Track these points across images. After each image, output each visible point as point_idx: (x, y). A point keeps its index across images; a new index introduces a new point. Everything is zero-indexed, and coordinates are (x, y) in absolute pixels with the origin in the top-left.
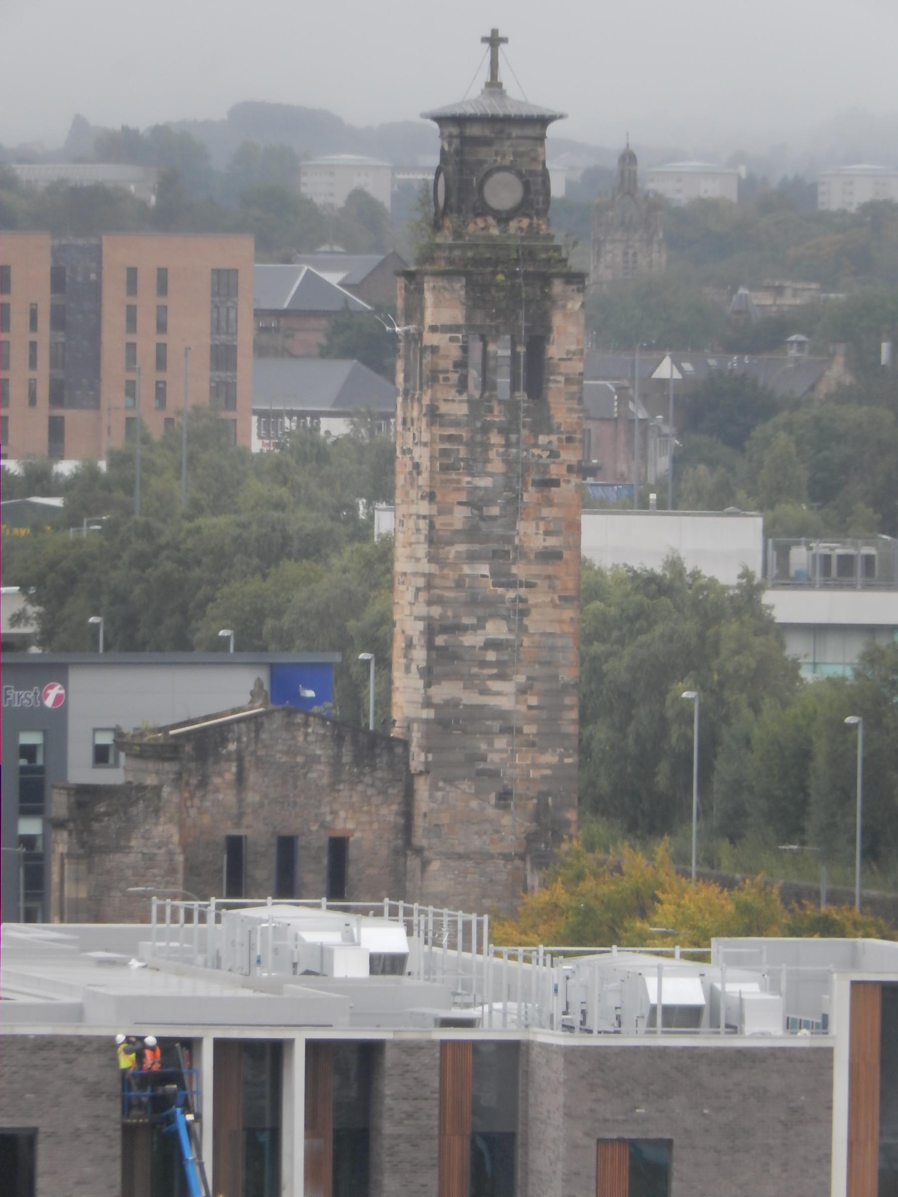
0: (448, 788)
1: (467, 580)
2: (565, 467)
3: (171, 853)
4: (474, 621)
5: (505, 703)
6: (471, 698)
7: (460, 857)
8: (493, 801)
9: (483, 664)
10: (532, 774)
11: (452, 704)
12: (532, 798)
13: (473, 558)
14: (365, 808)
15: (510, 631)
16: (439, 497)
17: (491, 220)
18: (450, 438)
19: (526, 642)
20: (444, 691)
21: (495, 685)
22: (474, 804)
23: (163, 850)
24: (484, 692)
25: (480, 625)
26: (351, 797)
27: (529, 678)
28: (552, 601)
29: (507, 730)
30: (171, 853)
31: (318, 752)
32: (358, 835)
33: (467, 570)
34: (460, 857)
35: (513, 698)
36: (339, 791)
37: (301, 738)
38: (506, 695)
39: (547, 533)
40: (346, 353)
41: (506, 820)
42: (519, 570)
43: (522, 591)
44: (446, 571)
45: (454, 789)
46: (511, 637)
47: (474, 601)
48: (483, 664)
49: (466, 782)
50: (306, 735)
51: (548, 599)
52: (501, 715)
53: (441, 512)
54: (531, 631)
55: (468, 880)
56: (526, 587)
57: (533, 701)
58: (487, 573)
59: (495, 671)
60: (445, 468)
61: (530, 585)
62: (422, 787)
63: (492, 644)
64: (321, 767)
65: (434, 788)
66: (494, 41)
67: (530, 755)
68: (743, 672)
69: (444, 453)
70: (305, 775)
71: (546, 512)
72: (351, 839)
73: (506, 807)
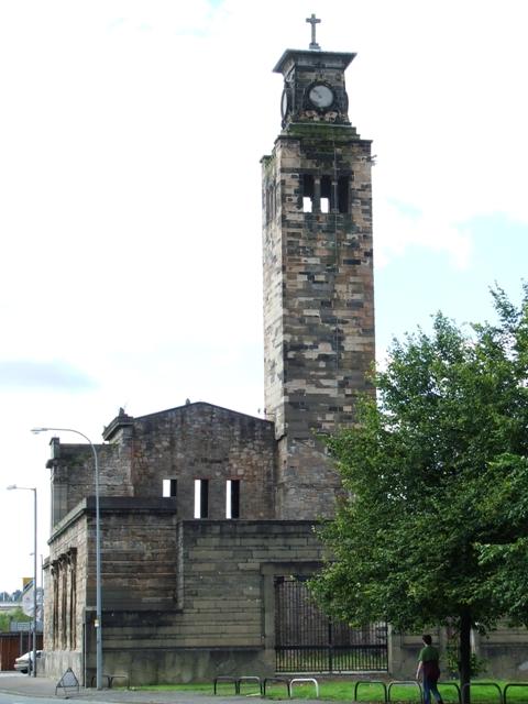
0: (298, 444)
4: (311, 343)
5: (333, 393)
6: (312, 390)
11: (301, 392)
13: (309, 306)
15: (333, 349)
16: (287, 270)
17: (314, 113)
18: (293, 234)
20: (296, 385)
21: (325, 382)
22: (315, 453)
24: (319, 386)
25: (315, 347)
27: (346, 378)
28: (358, 332)
29: (332, 409)
33: (306, 312)
34: (307, 486)
39: (354, 292)
40: (364, 141)
42: (339, 314)
43: (340, 326)
46: (334, 353)
47: (312, 329)
49: (113, 518)
51: (356, 330)
53: (289, 278)
54: (346, 349)
57: (349, 392)
59: (324, 373)
60: (291, 253)
61: (344, 322)
62: (283, 447)
63: (323, 357)
65: (290, 444)
66: (313, 21)
68: (439, 389)
69: (290, 243)
71: (352, 279)
73: (176, 510)
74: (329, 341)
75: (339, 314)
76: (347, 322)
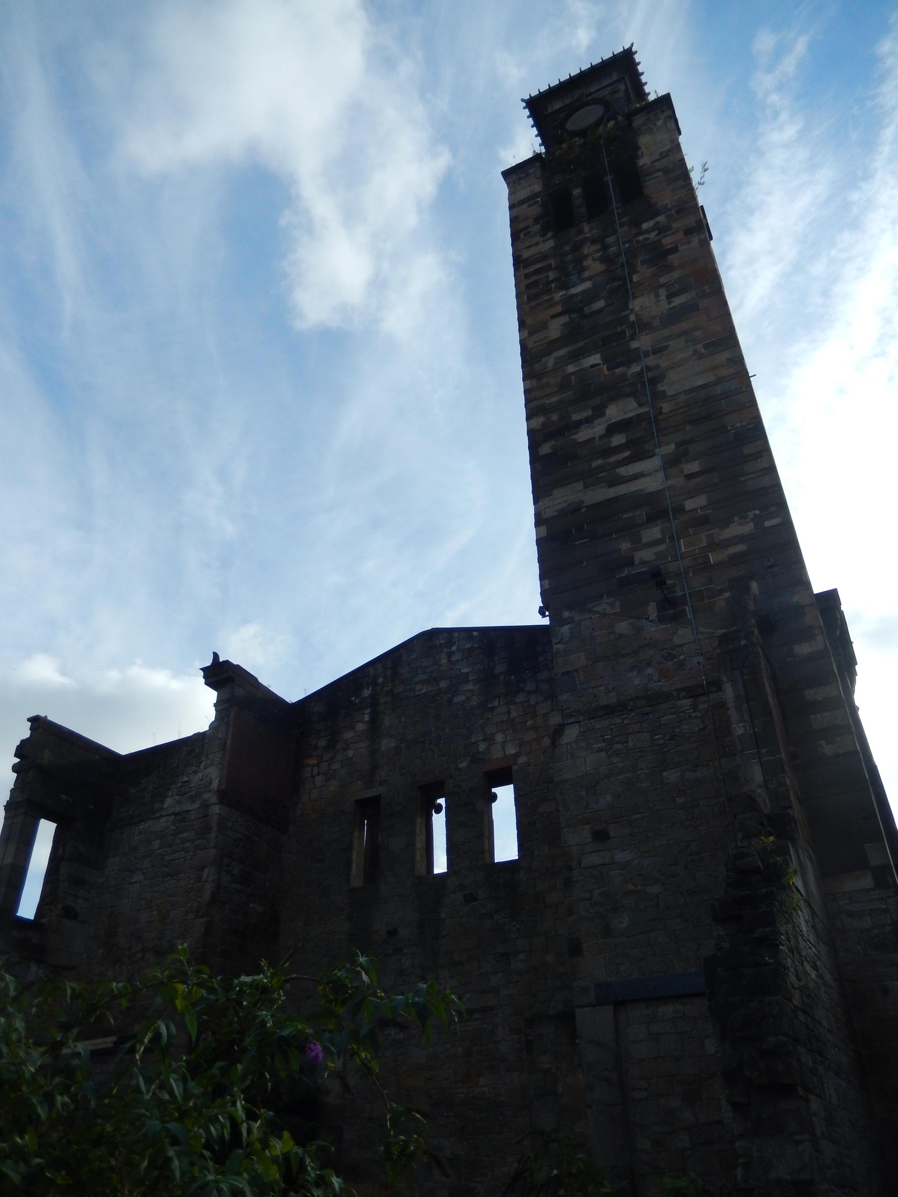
1: (573, 378)
2: (682, 233)
3: (206, 806)
5: (652, 484)
7: (609, 711)
8: (654, 615)
9: (610, 451)
10: (712, 559)
12: (721, 591)
14: (529, 723)
15: (641, 405)
19: (666, 407)
22: (623, 627)
23: (197, 805)
24: (614, 482)
25: (599, 412)
26: (509, 713)
27: (678, 445)
28: (695, 352)
30: (206, 806)
31: (465, 670)
32: (522, 760)
34: (609, 711)
35: (661, 475)
36: (493, 709)
37: (444, 661)
38: (650, 474)
41: (683, 635)
43: (651, 361)
44: (545, 380)
45: (587, 616)
46: (645, 409)
48: (610, 451)
50: (450, 654)
52: (650, 499)
55: (630, 744)
56: (654, 354)
57: (693, 467)
58: (600, 361)
64: (470, 686)
67: (703, 536)
70: (450, 701)
72: (515, 767)
74: (628, 395)
75: (643, 342)
76: (666, 348)
